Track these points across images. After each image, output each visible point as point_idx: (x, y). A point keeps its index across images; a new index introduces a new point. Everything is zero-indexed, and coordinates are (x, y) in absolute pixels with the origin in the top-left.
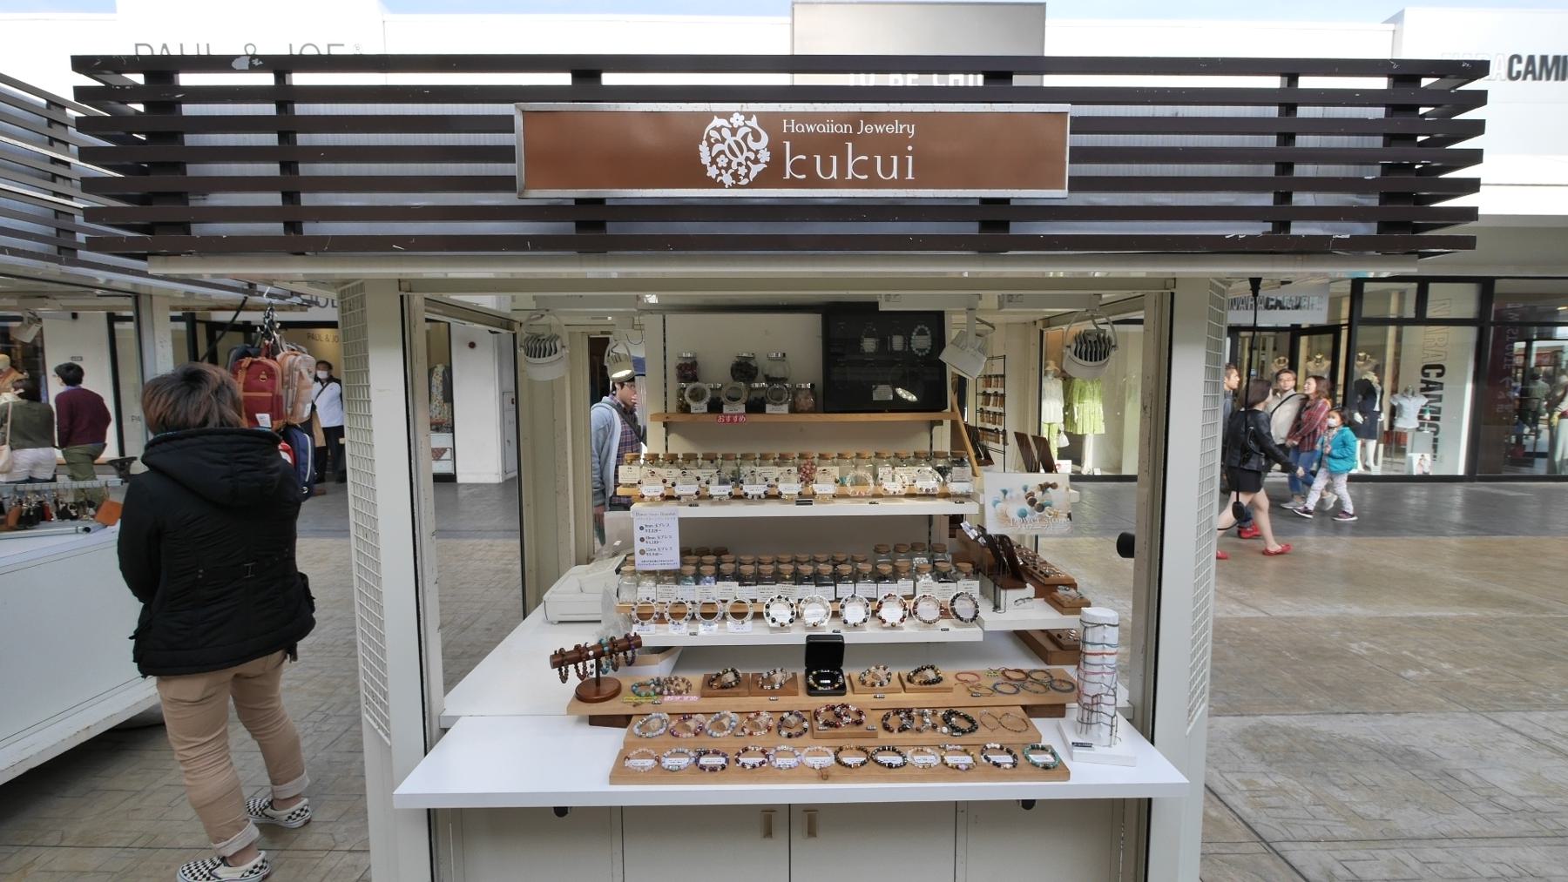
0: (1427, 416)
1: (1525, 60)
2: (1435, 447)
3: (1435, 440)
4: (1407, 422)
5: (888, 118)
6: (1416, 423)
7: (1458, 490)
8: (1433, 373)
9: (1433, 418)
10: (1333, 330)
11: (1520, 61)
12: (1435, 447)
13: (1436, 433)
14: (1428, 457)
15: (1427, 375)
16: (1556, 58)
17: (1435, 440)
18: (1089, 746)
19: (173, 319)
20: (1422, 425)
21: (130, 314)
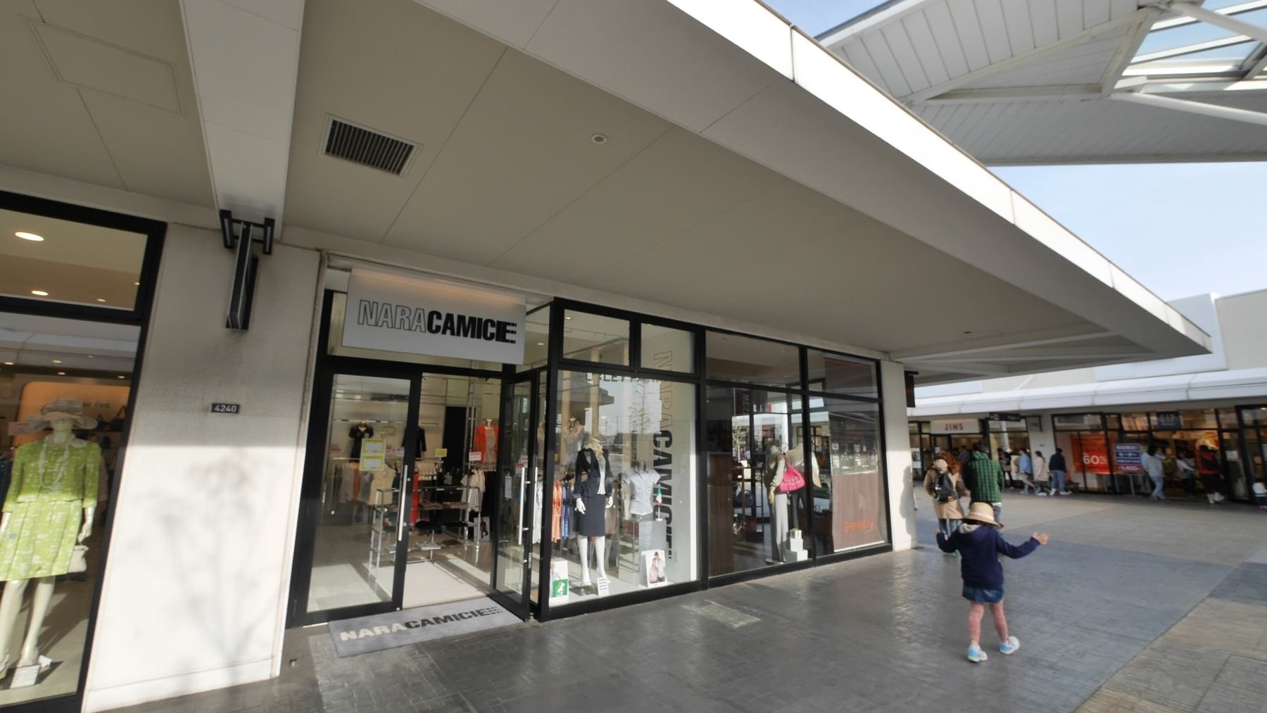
0: (659, 498)
1: (444, 317)
2: (669, 539)
3: (669, 530)
4: (641, 505)
5: (528, 521)
6: (649, 510)
7: (694, 609)
8: (436, 322)
9: (664, 500)
10: (531, 376)
11: (439, 317)
12: (669, 539)
13: (669, 520)
14: (662, 554)
15: (438, 328)
16: (472, 319)
17: (669, 530)
18: (237, 409)
19: (513, 332)
20: (656, 508)
21: (798, 388)
